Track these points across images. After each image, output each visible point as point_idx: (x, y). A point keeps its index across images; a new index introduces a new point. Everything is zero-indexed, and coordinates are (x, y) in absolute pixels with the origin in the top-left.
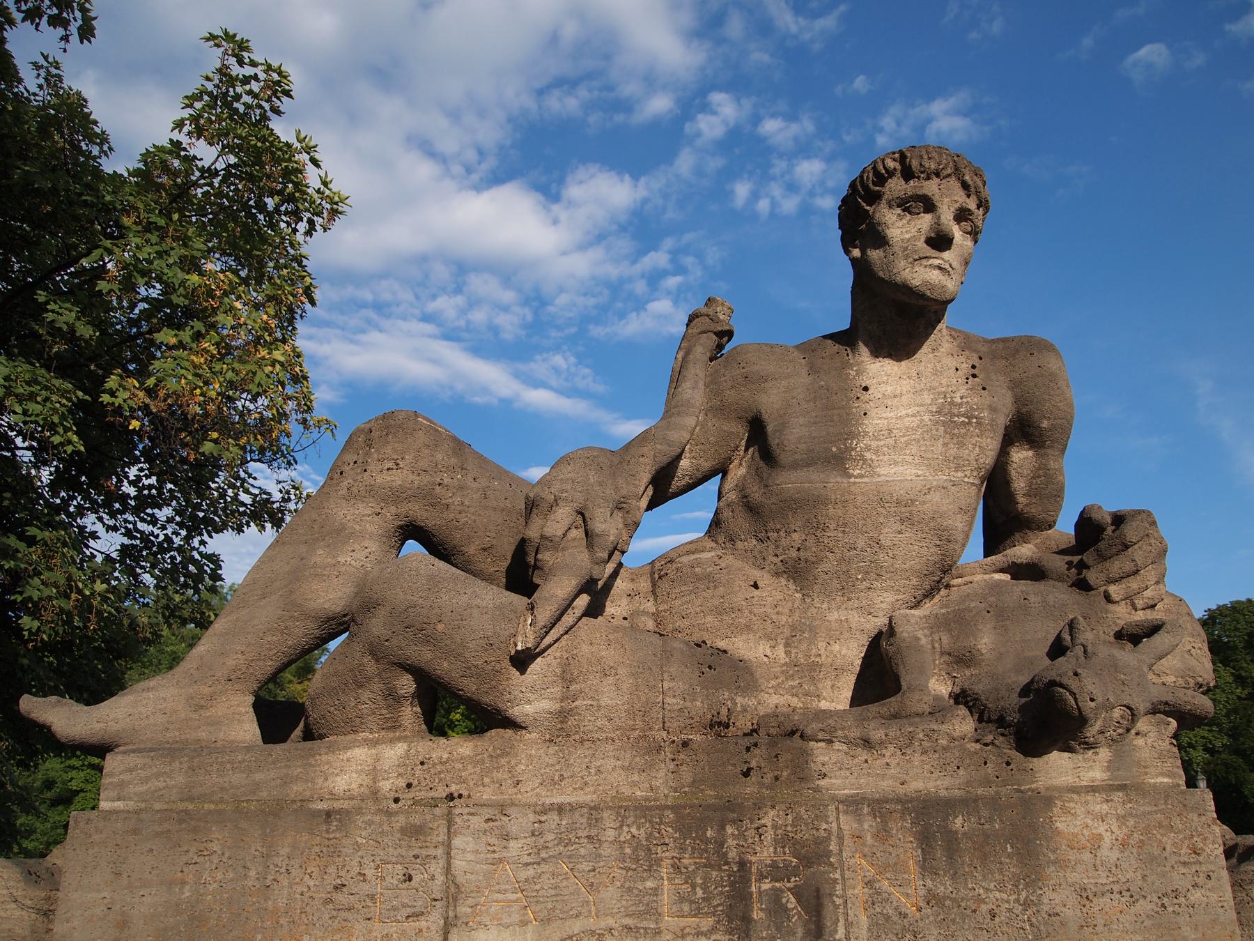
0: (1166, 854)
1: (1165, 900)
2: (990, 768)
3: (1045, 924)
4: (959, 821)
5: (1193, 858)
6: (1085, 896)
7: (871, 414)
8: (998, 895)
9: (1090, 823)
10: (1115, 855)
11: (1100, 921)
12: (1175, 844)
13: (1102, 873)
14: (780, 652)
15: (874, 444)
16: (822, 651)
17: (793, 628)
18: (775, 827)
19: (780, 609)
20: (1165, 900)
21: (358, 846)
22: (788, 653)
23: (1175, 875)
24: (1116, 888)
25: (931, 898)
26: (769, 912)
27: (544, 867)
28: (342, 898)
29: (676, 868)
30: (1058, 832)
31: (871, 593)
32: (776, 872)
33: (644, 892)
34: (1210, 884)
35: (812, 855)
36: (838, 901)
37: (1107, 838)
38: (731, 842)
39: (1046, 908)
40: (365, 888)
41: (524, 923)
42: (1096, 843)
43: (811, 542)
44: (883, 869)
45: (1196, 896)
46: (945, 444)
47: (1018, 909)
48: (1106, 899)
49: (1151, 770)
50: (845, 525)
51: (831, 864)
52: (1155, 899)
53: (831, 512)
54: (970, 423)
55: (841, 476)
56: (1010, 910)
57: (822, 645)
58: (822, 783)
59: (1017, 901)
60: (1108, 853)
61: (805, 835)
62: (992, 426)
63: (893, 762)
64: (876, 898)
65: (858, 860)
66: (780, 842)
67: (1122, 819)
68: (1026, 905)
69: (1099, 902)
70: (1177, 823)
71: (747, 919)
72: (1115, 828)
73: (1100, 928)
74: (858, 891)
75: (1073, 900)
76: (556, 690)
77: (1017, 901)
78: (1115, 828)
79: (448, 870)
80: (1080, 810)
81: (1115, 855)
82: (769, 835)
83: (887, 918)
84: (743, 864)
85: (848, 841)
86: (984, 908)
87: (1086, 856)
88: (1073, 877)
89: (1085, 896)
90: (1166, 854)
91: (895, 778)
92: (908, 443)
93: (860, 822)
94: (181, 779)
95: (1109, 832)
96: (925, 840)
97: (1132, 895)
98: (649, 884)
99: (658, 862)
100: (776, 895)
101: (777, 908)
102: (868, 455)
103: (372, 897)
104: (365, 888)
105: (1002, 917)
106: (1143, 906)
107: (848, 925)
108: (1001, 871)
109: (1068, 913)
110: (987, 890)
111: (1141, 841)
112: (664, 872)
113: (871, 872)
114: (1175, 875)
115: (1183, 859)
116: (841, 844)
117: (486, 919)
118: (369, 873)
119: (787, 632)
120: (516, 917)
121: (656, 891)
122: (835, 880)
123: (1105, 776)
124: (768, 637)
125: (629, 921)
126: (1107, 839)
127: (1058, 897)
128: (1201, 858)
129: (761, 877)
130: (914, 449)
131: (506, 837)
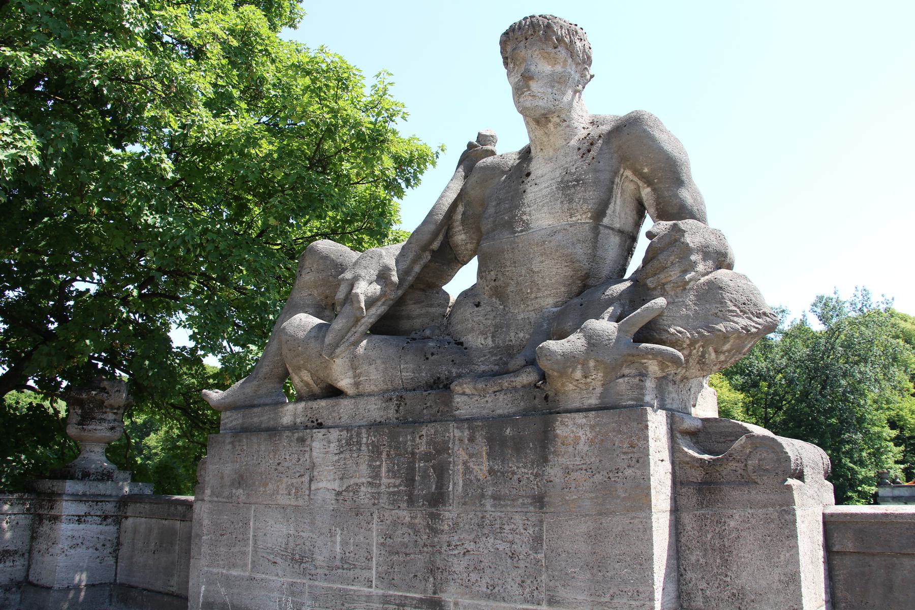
0: (615, 447)
1: (611, 475)
2: (537, 401)
3: (545, 486)
4: (508, 431)
5: (631, 450)
6: (567, 471)
7: (528, 191)
8: (523, 470)
9: (574, 429)
10: (586, 448)
11: (574, 485)
12: (621, 442)
13: (578, 459)
14: (490, 341)
15: (528, 209)
16: (513, 338)
17: (496, 326)
18: (427, 436)
19: (488, 317)
20: (611, 475)
21: (284, 447)
22: (493, 341)
23: (619, 460)
24: (584, 467)
25: (491, 471)
26: (422, 477)
27: (342, 456)
28: (279, 468)
29: (388, 455)
30: (556, 436)
31: (538, 300)
32: (427, 457)
33: (375, 467)
34: (638, 465)
35: (441, 448)
36: (451, 472)
37: (583, 438)
38: (409, 443)
39: (546, 477)
40: (286, 464)
41: (335, 480)
42: (577, 440)
43: (500, 276)
44: (471, 456)
45: (629, 472)
46: (562, 202)
47: (532, 478)
48: (578, 473)
49: (625, 397)
50: (515, 262)
51: (449, 454)
52: (605, 473)
53: (506, 256)
54: (578, 185)
55: (511, 233)
56: (528, 478)
57: (512, 334)
58: (457, 412)
59: (532, 473)
60: (583, 447)
61: (439, 439)
62: (594, 182)
63: (490, 400)
64: (467, 470)
65: (461, 452)
66: (428, 443)
67: (592, 427)
68: (536, 476)
69: (574, 475)
70: (624, 428)
71: (413, 480)
72: (588, 433)
73: (573, 489)
74: (460, 468)
75: (560, 474)
76: (350, 373)
77: (532, 473)
78: (588, 433)
79: (311, 457)
80: (570, 423)
81: (586, 448)
82: (424, 439)
83: (471, 481)
84: (413, 454)
85: (457, 442)
86: (516, 477)
87: (571, 449)
88: (561, 460)
89: (567, 471)
90: (615, 447)
91: (489, 408)
92: (543, 206)
93: (462, 432)
94: (240, 421)
95: (584, 435)
96: (490, 441)
97: (591, 470)
98: (378, 463)
99: (381, 453)
100: (426, 470)
101: (425, 476)
102: (525, 218)
103: (288, 468)
104: (286, 464)
105: (524, 482)
106: (598, 478)
107: (454, 484)
108: (526, 457)
109: (557, 480)
110: (518, 468)
111: (602, 440)
112: (384, 456)
113: (466, 457)
114: (619, 460)
115: (624, 450)
116: (454, 443)
117: (322, 478)
118: (287, 457)
119: (492, 329)
120: (332, 477)
121: (380, 466)
122: (450, 462)
123: (597, 402)
124: (482, 333)
125: (369, 480)
126: (583, 438)
127: (554, 472)
128: (635, 450)
129: (420, 460)
130: (546, 208)
131: (329, 442)
